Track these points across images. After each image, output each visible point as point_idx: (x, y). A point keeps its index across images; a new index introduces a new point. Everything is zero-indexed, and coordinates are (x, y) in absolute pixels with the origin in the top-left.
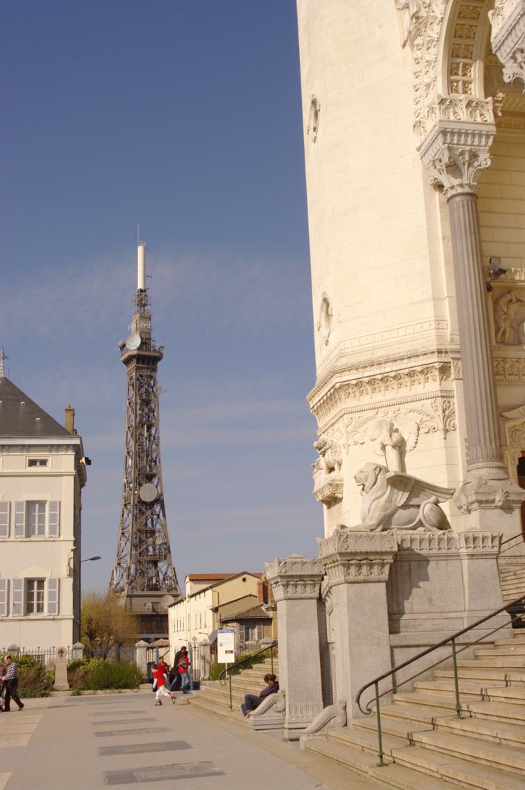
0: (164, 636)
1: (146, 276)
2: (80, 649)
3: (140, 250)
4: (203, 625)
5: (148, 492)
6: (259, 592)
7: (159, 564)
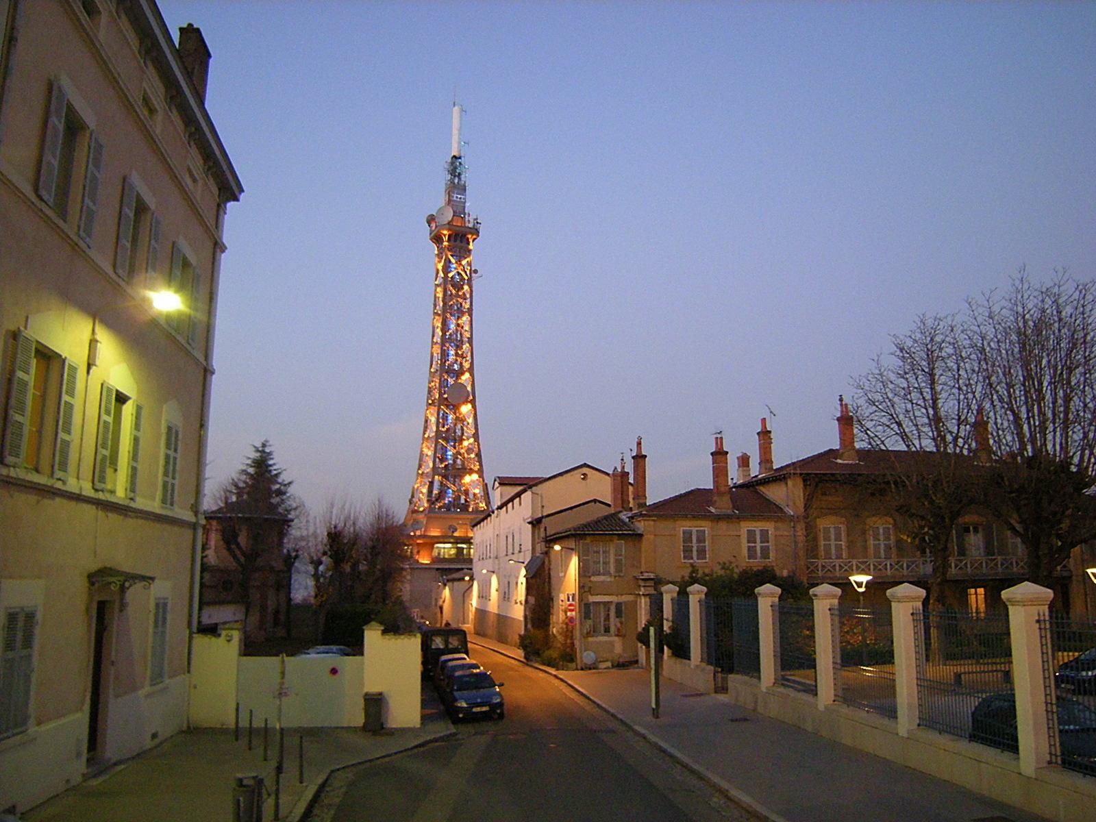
0: (470, 567)
2: (976, 591)
4: (516, 551)
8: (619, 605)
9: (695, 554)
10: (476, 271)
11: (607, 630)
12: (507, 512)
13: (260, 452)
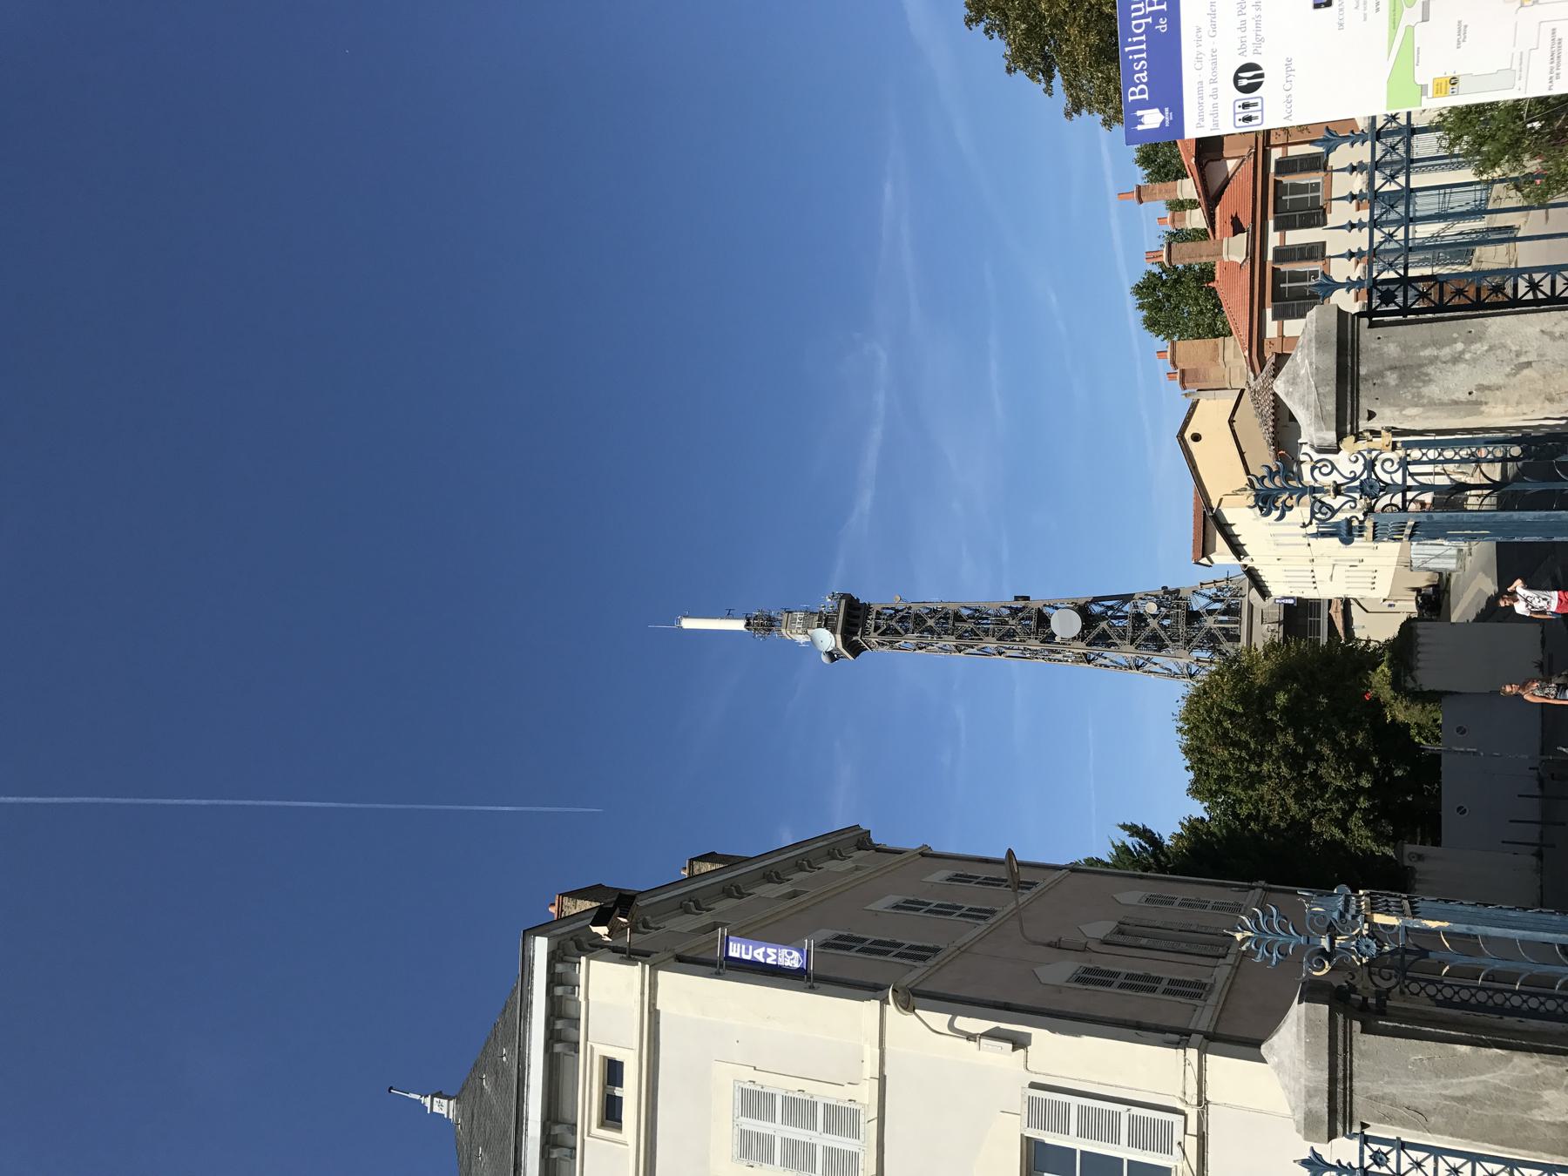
1: (730, 615)
3: (688, 624)
5: (1066, 624)
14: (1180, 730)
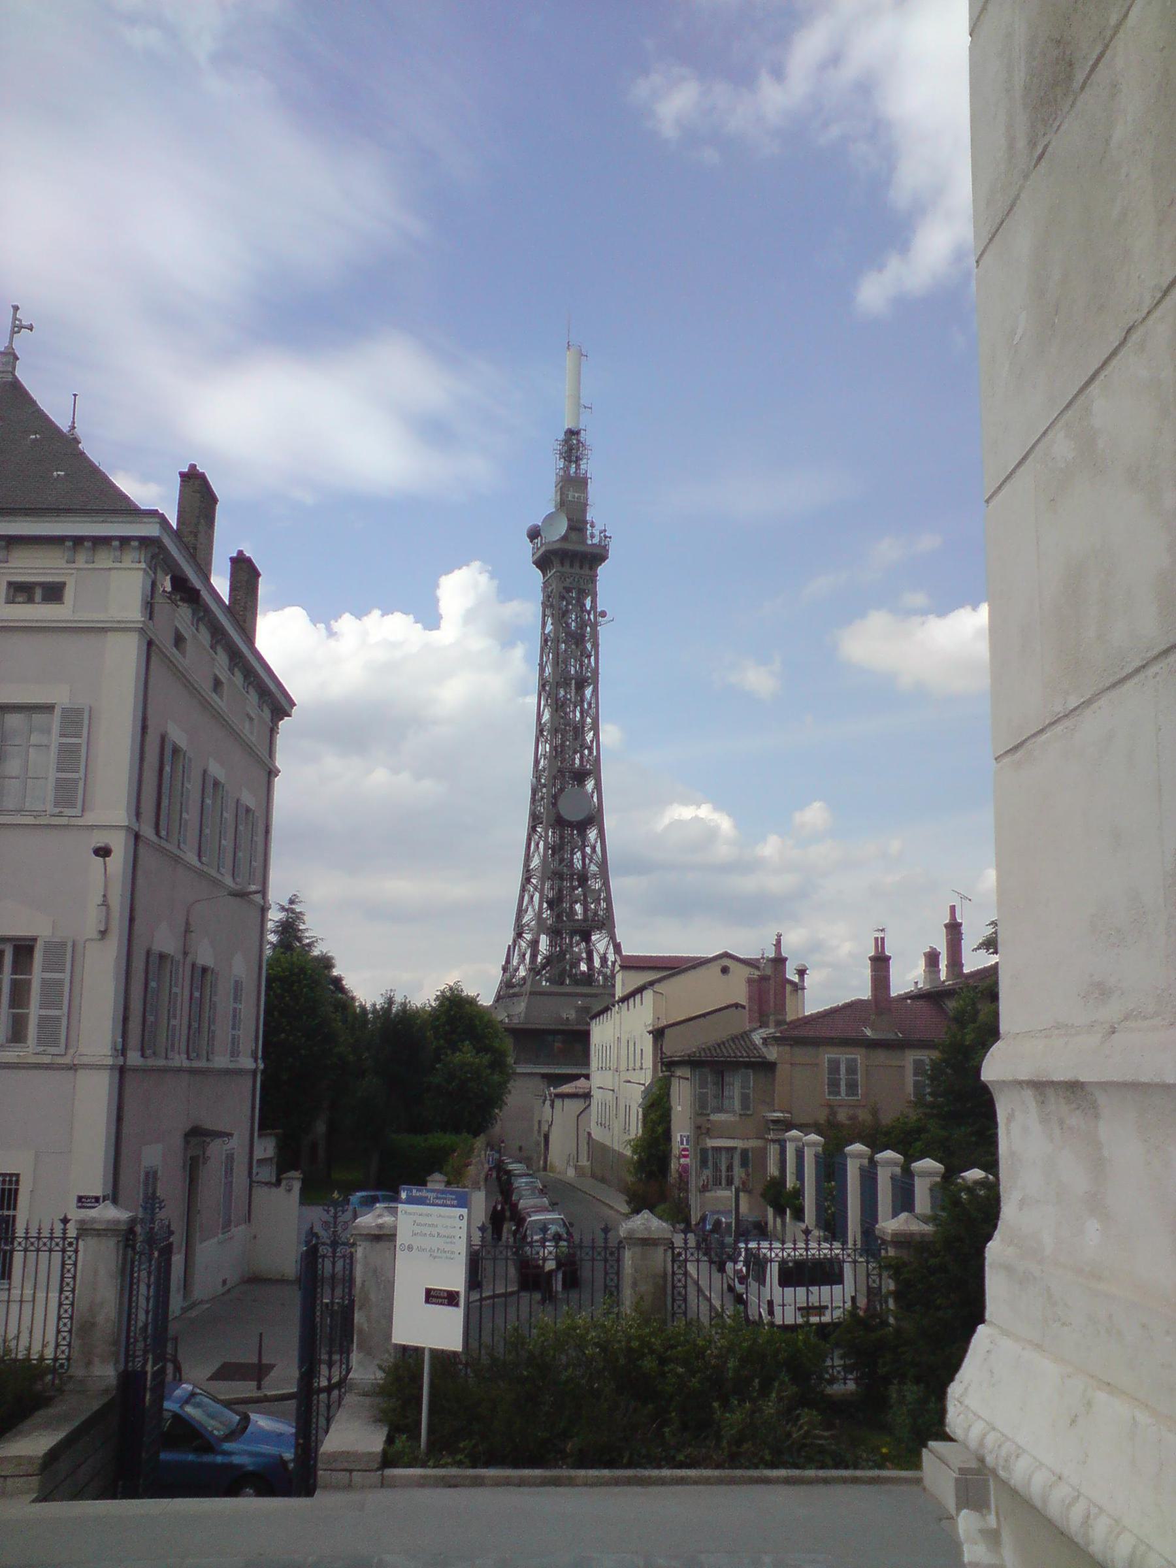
6: (750, 999)
7: (593, 938)
8: (744, 1153)
9: (843, 1088)
10: (603, 614)
11: (730, 1182)
12: (628, 1009)
13: (287, 910)
14: (390, 1001)
